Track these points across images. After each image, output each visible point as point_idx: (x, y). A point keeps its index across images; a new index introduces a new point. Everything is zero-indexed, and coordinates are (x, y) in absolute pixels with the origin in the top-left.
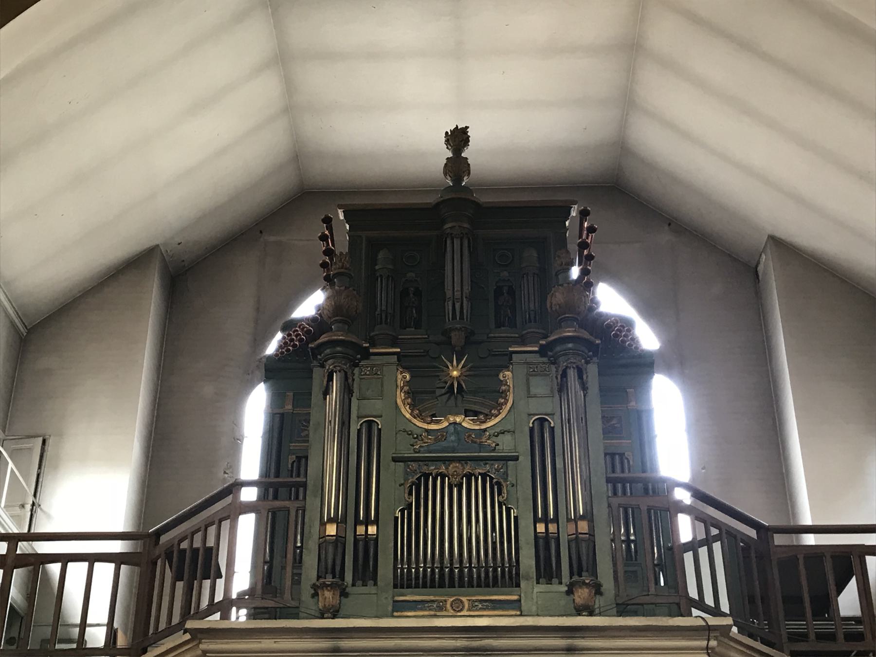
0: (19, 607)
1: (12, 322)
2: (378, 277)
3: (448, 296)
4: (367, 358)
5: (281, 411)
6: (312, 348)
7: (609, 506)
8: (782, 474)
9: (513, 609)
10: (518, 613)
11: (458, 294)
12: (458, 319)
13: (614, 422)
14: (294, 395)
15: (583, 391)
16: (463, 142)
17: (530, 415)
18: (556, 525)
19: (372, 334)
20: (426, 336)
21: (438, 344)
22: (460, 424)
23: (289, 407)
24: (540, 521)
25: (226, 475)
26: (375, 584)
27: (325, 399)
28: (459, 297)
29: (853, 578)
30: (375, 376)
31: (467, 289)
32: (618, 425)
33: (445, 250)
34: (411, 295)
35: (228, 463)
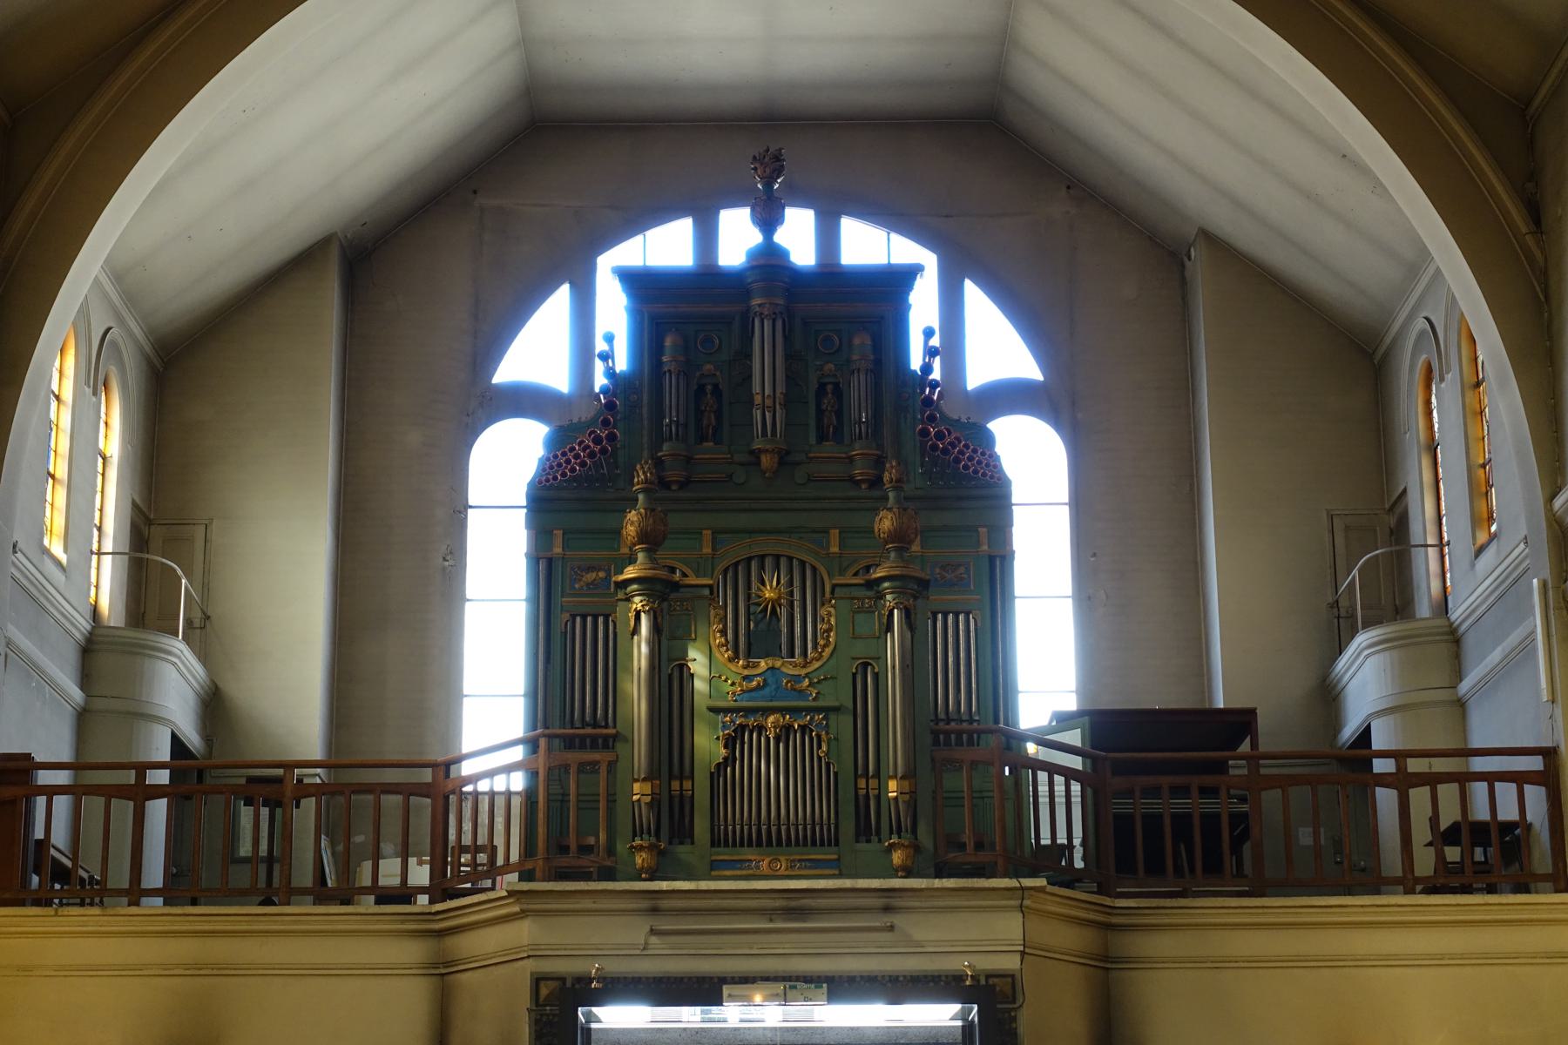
0: (198, 752)
1: (115, 311)
2: (665, 372)
3: (756, 403)
4: (677, 591)
5: (549, 554)
6: (616, 583)
7: (933, 760)
8: (1196, 563)
9: (832, 868)
10: (837, 872)
11: (768, 402)
12: (769, 435)
13: (962, 570)
14: (563, 534)
15: (911, 632)
16: (777, 172)
17: (853, 659)
18: (877, 781)
19: (660, 454)
20: (729, 456)
21: (742, 464)
22: (778, 669)
23: (558, 550)
24: (861, 776)
25: (447, 563)
26: (693, 843)
27: (632, 638)
28: (771, 405)
29: (1246, 741)
30: (686, 612)
31: (780, 389)
32: (965, 576)
33: (753, 332)
34: (709, 396)
35: (448, 546)
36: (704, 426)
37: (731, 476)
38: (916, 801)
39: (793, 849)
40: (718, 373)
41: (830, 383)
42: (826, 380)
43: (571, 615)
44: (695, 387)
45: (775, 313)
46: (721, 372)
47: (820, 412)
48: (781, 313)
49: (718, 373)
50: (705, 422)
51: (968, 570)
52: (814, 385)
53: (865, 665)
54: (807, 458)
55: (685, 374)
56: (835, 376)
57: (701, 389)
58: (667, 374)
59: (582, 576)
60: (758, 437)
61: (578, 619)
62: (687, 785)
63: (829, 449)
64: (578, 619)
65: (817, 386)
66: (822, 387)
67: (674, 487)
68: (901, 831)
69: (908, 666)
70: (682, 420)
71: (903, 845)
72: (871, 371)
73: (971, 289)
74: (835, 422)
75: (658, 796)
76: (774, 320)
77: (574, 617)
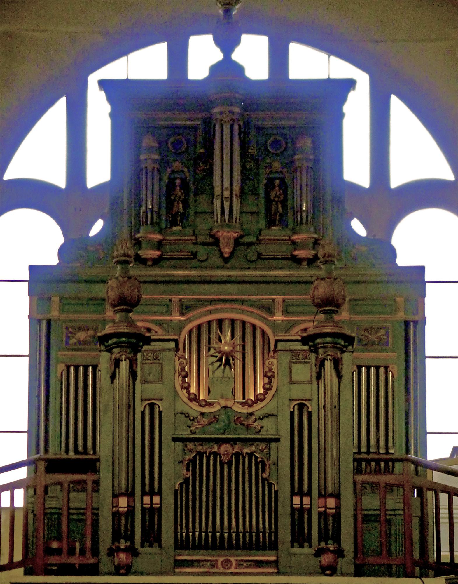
17: (290, 400)
31: (236, 187)
45: (232, 119)
49: (185, 170)
50: (175, 209)
51: (387, 333)
57: (171, 186)
66: (270, 185)
69: (335, 407)
70: (156, 209)
74: (281, 212)
77: (68, 367)
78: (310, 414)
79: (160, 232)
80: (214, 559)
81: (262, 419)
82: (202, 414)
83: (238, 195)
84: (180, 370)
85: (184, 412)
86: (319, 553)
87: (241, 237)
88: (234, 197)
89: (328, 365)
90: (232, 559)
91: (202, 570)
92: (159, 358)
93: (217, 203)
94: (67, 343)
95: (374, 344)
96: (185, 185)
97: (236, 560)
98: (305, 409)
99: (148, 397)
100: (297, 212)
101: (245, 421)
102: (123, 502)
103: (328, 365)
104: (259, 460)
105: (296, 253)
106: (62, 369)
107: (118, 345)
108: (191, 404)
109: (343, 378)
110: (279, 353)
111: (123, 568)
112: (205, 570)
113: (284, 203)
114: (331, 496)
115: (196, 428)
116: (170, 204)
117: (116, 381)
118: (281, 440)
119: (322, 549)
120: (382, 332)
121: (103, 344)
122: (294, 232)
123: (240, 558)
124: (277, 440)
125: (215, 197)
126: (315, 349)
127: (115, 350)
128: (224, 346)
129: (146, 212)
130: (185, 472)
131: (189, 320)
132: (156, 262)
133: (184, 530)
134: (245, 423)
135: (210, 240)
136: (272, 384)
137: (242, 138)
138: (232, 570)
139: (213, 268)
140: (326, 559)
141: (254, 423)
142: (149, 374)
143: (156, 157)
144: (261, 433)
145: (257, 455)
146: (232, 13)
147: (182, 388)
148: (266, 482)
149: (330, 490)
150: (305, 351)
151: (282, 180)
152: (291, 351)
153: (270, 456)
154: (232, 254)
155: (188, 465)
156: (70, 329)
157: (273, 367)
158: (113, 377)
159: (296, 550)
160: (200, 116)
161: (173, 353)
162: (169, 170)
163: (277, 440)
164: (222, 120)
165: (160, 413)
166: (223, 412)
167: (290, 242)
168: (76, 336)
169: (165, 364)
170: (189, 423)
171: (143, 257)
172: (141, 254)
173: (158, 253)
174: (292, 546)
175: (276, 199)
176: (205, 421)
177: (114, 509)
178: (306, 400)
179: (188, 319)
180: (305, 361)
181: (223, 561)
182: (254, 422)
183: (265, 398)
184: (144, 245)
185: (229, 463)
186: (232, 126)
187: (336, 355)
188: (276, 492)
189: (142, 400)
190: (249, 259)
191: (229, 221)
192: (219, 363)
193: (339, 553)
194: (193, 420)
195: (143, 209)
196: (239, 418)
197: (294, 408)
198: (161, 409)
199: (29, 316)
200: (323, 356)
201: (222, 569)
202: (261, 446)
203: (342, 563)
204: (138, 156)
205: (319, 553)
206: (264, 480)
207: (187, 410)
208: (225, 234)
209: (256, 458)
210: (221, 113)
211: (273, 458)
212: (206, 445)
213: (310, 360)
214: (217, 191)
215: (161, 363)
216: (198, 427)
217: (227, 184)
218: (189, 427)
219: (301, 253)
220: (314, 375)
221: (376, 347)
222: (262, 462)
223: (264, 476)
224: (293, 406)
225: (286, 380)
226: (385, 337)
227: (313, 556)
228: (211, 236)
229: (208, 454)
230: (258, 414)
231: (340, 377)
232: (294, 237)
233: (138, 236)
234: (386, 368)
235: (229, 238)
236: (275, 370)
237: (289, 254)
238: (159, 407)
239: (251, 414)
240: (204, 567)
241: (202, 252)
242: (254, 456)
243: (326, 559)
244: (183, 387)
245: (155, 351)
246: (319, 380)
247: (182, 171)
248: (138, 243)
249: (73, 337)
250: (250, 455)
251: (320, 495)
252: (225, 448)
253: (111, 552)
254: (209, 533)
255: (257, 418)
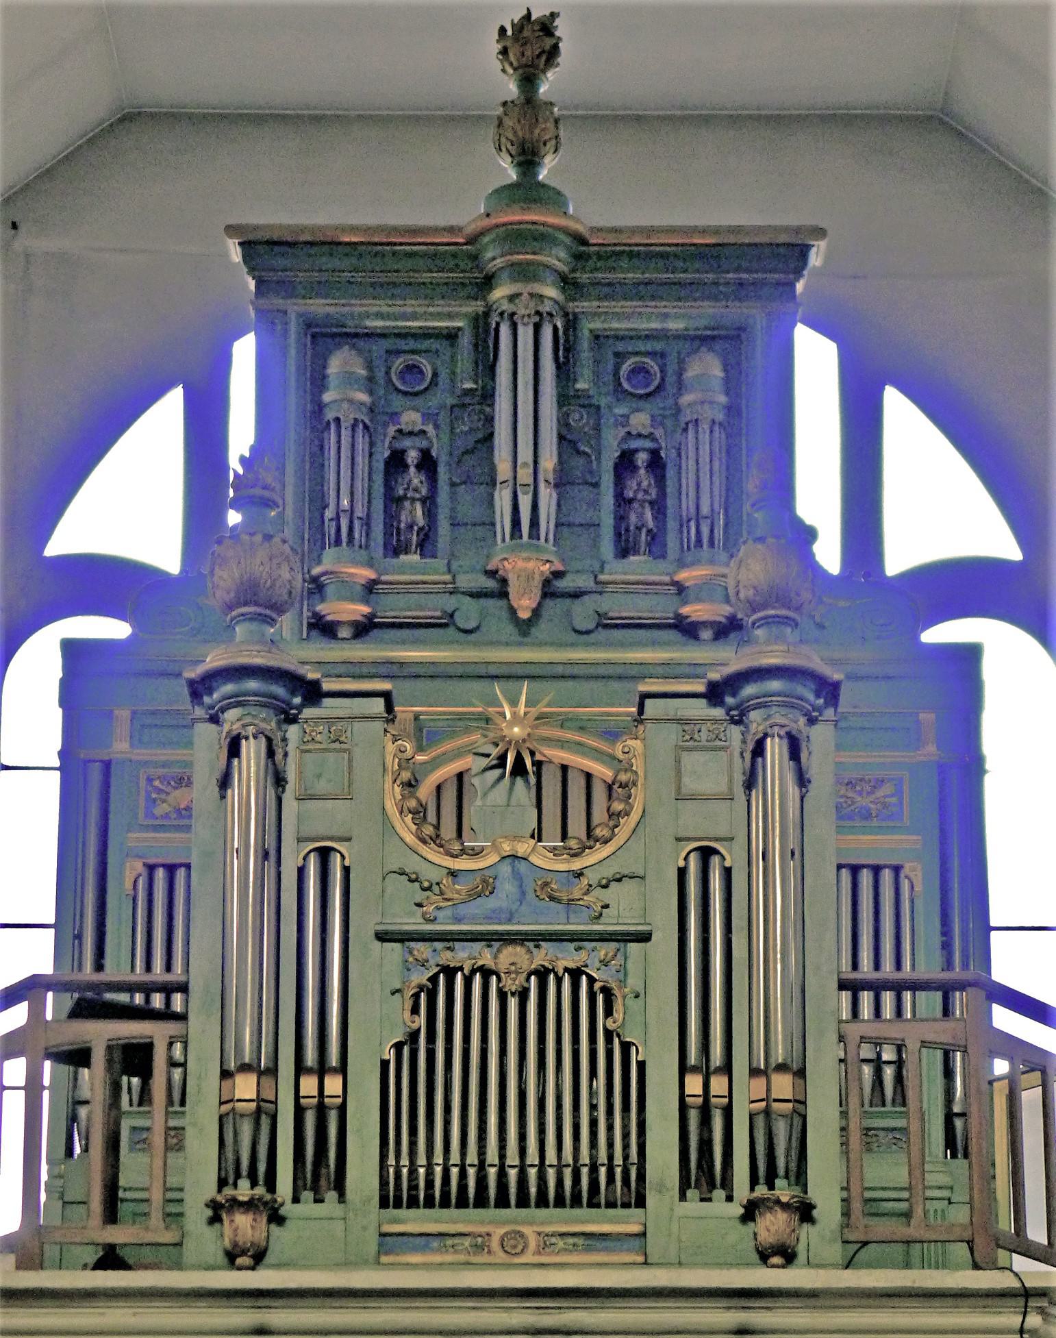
2: (328, 423)
3: (500, 478)
17: (679, 840)
24: (695, 1069)
31: (549, 462)
36: (403, 525)
37: (452, 616)
38: (804, 1117)
39: (552, 1212)
40: (430, 429)
41: (644, 449)
42: (634, 444)
43: (144, 864)
44: (387, 454)
45: (538, 313)
46: (436, 427)
47: (622, 501)
48: (550, 314)
49: (430, 429)
50: (404, 517)
51: (899, 793)
52: (610, 456)
53: (706, 853)
54: (597, 583)
55: (366, 427)
56: (651, 437)
57: (396, 462)
58: (333, 427)
59: (168, 794)
60: (504, 540)
61: (160, 874)
62: (333, 1085)
63: (638, 566)
64: (160, 874)
65: (617, 454)
66: (625, 463)
67: (344, 633)
68: (776, 1176)
69: (793, 854)
70: (360, 512)
71: (778, 1202)
72: (720, 424)
73: (896, 405)
74: (651, 524)
75: (272, 1106)
76: (537, 328)
77: (151, 868)
78: (727, 872)
79: (370, 564)
80: (483, 1229)
81: (606, 886)
82: (453, 874)
83: (552, 481)
84: (396, 767)
85: (407, 870)
86: (751, 1212)
87: (558, 575)
88: (542, 485)
89: (775, 750)
90: (527, 1231)
91: (449, 1258)
92: (342, 739)
93: (503, 499)
94: (149, 814)
95: (867, 815)
96: (427, 463)
97: (539, 1234)
98: (715, 860)
99: (313, 835)
100: (689, 521)
101: (560, 892)
102: (245, 1087)
103: (775, 750)
104: (597, 986)
105: (685, 610)
106: (134, 874)
107: (237, 701)
108: (424, 850)
109: (811, 787)
110: (649, 725)
111: (243, 1253)
112: (462, 1258)
113: (659, 507)
114: (782, 1068)
115: (438, 908)
116: (393, 501)
117: (234, 793)
118: (654, 938)
119: (763, 1201)
120: (887, 789)
121: (201, 704)
122: (682, 564)
123: (549, 1229)
124: (645, 938)
125: (498, 485)
126: (738, 718)
127: (232, 715)
128: (512, 724)
129: (337, 518)
130: (407, 1014)
131: (435, 764)
132: (363, 629)
133: (405, 1161)
134: (563, 895)
135: (491, 584)
136: (634, 768)
137: (562, 359)
138: (528, 1258)
139: (492, 644)
140: (772, 1226)
141: (585, 898)
142: (319, 776)
143: (363, 397)
144: (602, 920)
145: (594, 975)
146: (538, 89)
147: (401, 812)
148: (616, 1041)
149: (779, 1055)
150: (715, 721)
151: (655, 454)
152: (679, 721)
153: (626, 975)
154: (536, 612)
155: (416, 996)
156: (157, 783)
157: (633, 761)
158: (225, 782)
159: (693, 1206)
160: (464, 309)
161: (379, 726)
162: (392, 430)
163: (645, 938)
164: (513, 314)
165: (346, 870)
166: (505, 869)
167: (673, 589)
168: (170, 798)
169: (357, 752)
170: (420, 896)
171: (329, 618)
172: (323, 613)
173: (366, 609)
174: (683, 1197)
175: (640, 496)
176: (461, 888)
177: (225, 1108)
178: (716, 840)
179: (434, 759)
180: (716, 745)
181: (506, 1234)
182: (587, 893)
183: (613, 835)
184: (330, 590)
185: (523, 995)
186: (537, 328)
187: (793, 725)
188: (642, 1065)
189: (299, 840)
190: (578, 628)
191: (530, 537)
192: (498, 772)
193: (805, 1212)
194: (429, 889)
195: (329, 514)
196: (546, 884)
197: (686, 859)
198: (347, 863)
199: (60, 753)
200: (761, 728)
201: (502, 1254)
202: (603, 953)
203: (809, 1238)
204: (480, 1236)
205: (751, 1212)
206: (609, 1035)
207: (413, 864)
208: (520, 564)
209: (591, 980)
210: (512, 298)
211: (634, 982)
212: (463, 949)
213: (727, 743)
214: (503, 469)
215: (348, 750)
216: (441, 904)
217: (525, 454)
218: (419, 905)
219: (694, 611)
220: (739, 779)
221: (875, 823)
222: (606, 991)
223: (611, 1025)
224: (685, 856)
225: (669, 792)
226: (894, 800)
227: (738, 1221)
228: (492, 574)
229: (466, 971)
230: (592, 877)
231: (802, 781)
232: (682, 576)
233: (316, 571)
234: (897, 869)
235: (530, 577)
236: (638, 765)
237: (671, 615)
238: (343, 857)
239: (579, 874)
240: (456, 1252)
241: (469, 613)
242: (584, 977)
243: (772, 1226)
244: (405, 809)
245: (330, 720)
246: (750, 791)
247: (424, 432)
248: (317, 587)
249: (164, 801)
250: (575, 974)
251: (754, 1072)
252: (510, 957)
253: (217, 1213)
254: (468, 1168)
255: (594, 884)
